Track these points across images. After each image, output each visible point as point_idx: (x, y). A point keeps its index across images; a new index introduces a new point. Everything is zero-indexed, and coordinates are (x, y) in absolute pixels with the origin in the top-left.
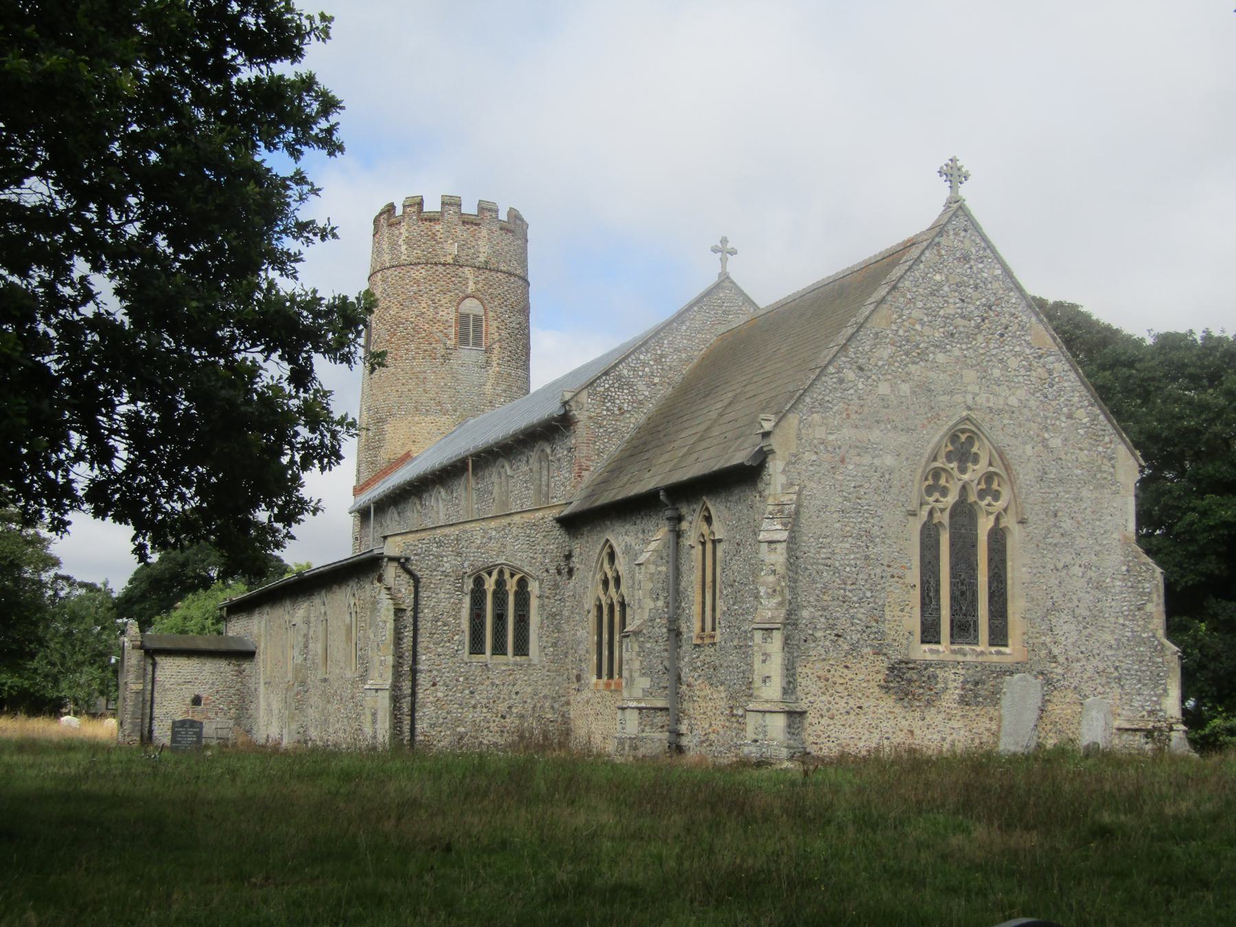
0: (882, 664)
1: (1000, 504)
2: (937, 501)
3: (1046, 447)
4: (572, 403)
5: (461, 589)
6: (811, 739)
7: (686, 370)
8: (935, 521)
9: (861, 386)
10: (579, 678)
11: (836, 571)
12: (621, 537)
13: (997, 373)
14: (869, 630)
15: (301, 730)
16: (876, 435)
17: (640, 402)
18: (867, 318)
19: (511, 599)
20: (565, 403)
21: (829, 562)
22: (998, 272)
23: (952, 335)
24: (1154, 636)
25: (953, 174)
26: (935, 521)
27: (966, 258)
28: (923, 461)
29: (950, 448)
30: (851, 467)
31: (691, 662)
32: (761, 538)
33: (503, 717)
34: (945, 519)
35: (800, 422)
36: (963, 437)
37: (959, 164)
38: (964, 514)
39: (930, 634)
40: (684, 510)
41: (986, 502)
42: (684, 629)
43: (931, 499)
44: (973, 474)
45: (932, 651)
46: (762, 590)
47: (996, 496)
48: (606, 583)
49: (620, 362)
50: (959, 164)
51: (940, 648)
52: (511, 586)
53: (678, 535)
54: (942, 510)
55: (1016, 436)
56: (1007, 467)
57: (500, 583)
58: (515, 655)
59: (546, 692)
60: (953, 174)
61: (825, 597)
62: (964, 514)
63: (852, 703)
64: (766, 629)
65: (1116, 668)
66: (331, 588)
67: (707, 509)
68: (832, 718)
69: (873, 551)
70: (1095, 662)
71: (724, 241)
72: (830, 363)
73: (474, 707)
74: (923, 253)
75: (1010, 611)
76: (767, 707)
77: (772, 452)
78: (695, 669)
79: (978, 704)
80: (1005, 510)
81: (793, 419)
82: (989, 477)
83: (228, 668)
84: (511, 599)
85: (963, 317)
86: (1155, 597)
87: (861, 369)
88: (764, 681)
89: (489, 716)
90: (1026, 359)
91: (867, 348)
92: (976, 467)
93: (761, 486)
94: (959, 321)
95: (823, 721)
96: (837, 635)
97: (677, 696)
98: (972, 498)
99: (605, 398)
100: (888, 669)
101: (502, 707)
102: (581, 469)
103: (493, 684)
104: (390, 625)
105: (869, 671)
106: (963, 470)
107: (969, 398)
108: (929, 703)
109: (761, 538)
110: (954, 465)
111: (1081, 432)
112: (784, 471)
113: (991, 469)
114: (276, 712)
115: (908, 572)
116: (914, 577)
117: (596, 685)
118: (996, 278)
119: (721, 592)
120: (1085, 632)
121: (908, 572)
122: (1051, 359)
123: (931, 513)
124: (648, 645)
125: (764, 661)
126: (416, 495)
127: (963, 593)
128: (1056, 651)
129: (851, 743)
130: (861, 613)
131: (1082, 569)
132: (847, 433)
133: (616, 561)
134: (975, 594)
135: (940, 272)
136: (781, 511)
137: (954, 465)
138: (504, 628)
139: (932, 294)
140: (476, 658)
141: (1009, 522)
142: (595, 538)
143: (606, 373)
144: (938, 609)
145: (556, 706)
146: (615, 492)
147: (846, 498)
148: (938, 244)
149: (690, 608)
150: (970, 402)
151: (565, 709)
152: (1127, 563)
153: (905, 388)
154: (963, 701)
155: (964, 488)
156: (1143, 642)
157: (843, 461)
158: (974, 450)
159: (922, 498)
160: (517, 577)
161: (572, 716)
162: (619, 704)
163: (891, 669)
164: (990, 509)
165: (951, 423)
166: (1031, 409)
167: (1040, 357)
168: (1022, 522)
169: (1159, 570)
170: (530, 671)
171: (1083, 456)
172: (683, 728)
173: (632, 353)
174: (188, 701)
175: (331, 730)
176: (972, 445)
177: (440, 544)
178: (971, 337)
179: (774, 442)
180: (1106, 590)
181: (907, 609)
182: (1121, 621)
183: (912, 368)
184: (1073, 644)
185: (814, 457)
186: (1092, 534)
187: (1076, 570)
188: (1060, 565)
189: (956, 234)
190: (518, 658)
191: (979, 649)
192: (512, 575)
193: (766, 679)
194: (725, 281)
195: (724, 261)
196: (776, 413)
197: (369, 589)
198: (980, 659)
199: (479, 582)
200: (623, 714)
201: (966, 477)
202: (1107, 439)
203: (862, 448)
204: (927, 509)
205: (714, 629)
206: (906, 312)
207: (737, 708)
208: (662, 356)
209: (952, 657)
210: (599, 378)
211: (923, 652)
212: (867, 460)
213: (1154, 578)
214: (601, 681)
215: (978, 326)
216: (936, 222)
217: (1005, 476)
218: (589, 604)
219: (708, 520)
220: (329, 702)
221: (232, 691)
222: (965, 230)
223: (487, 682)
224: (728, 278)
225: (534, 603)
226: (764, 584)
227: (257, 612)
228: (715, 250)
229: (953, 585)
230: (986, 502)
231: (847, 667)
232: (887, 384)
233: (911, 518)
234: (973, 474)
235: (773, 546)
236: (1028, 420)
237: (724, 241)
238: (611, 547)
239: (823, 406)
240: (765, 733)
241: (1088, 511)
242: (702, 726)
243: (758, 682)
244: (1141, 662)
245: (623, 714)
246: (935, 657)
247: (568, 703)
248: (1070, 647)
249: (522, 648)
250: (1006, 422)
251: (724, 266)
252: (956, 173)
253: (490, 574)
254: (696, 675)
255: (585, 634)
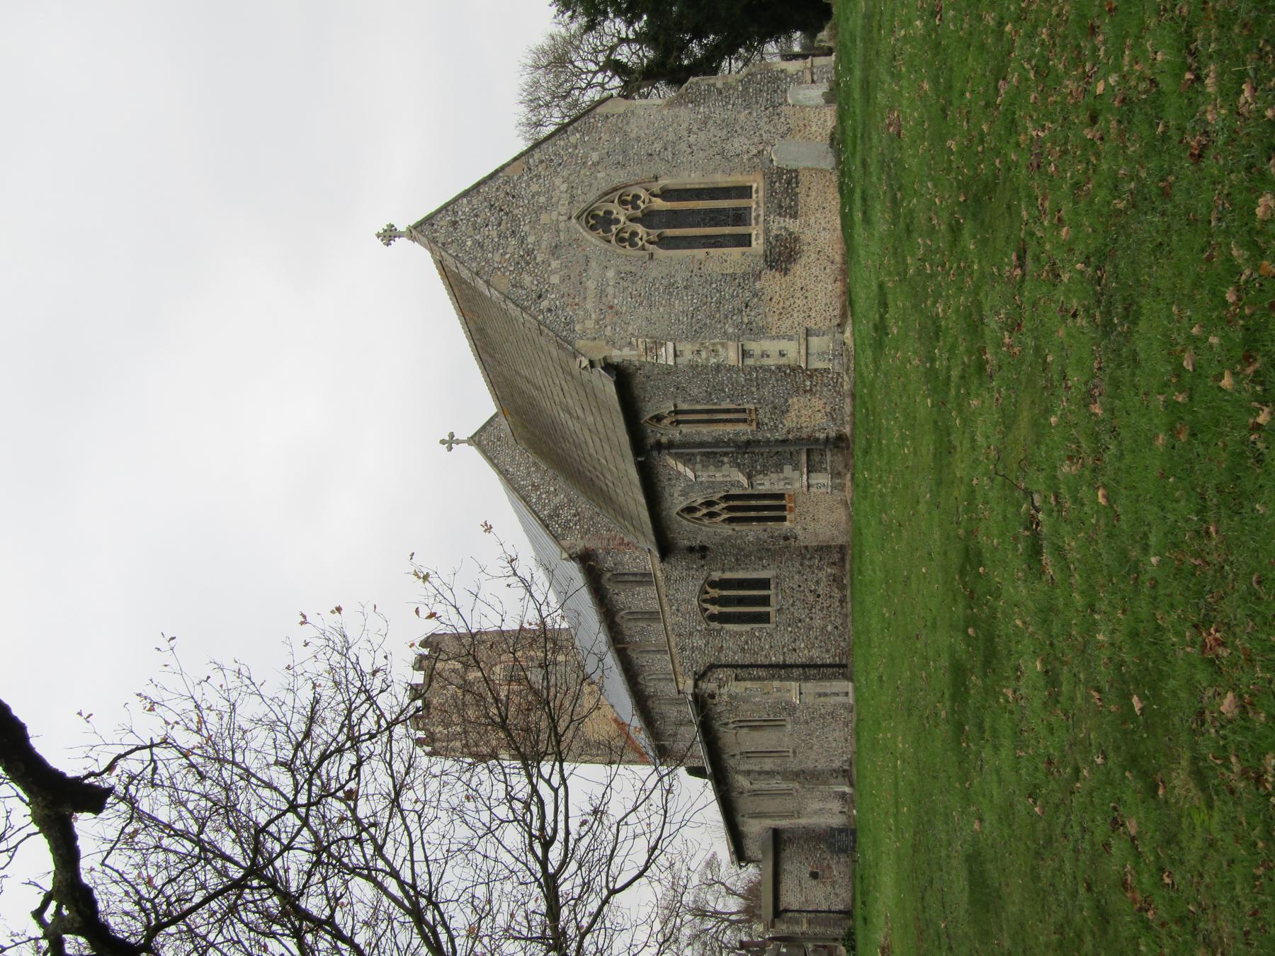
0: (768, 274)
1: (643, 194)
2: (641, 239)
3: (598, 163)
4: (571, 552)
5: (719, 632)
6: (827, 323)
7: (543, 466)
8: (656, 239)
9: (553, 296)
10: (786, 538)
11: (697, 309)
12: (675, 501)
13: (542, 199)
14: (742, 285)
15: (835, 775)
16: (591, 284)
17: (570, 501)
18: (500, 293)
19: (725, 593)
20: (571, 557)
21: (690, 316)
22: (465, 201)
23: (513, 232)
24: (741, 81)
25: (389, 235)
26: (656, 239)
27: (455, 223)
28: (610, 249)
29: (600, 230)
30: (616, 301)
31: (770, 430)
32: (672, 364)
33: (819, 596)
34: (655, 233)
35: (581, 338)
36: (592, 222)
37: (381, 231)
38: (649, 218)
39: (744, 241)
40: (651, 441)
41: (641, 205)
42: (744, 438)
43: (640, 243)
44: (620, 213)
45: (756, 240)
46: (713, 361)
47: (637, 197)
48: (711, 515)
49: (538, 517)
50: (381, 231)
51: (754, 233)
52: (715, 593)
53: (671, 445)
54: (648, 234)
55: (590, 185)
56: (615, 190)
57: (713, 601)
58: (769, 589)
59: (797, 565)
60: (389, 235)
61: (717, 316)
62: (649, 218)
63: (798, 294)
64: (743, 355)
65: (766, 109)
66: (720, 748)
67: (651, 419)
68: (811, 309)
69: (681, 284)
70: (762, 123)
71: (443, 442)
72: (535, 319)
73: (811, 619)
74: (450, 255)
75: (725, 185)
76: (803, 352)
77: (605, 359)
78: (776, 427)
79: (796, 205)
80: (647, 190)
81: (580, 344)
82: (623, 202)
83: (788, 851)
84: (725, 593)
85: (499, 225)
86: (711, 81)
87: (540, 297)
88: (784, 355)
89: (818, 607)
90: (531, 179)
91: (524, 292)
92: (615, 212)
93: (632, 369)
94: (503, 227)
95: (813, 315)
96: (746, 307)
97: (799, 441)
98: (639, 213)
99: (566, 527)
100: (771, 270)
101: (811, 598)
102: (622, 543)
103: (793, 605)
104: (749, 684)
105: (772, 283)
106: (617, 221)
107: (561, 218)
108: (797, 240)
109: (672, 364)
110: (613, 228)
111: (586, 139)
112: (620, 349)
113: (616, 201)
114: (821, 805)
115: (697, 257)
116: (700, 253)
117: (791, 521)
118: (469, 202)
119: (715, 404)
120: (739, 131)
121: (697, 257)
122: (531, 161)
123: (651, 243)
124: (759, 467)
125: (768, 356)
126: (646, 701)
127: (712, 219)
128: (755, 152)
129: (829, 294)
130: (728, 291)
131: (691, 135)
132: (589, 305)
133: (694, 505)
134: (712, 211)
135: (464, 243)
136: (651, 349)
137: (613, 228)
138: (749, 597)
139: (482, 247)
140: (773, 619)
141: (656, 188)
142: (676, 526)
143: (547, 526)
144: (724, 236)
145: (808, 556)
146: (640, 509)
147: (641, 304)
148: (443, 244)
149: (729, 433)
150: (565, 218)
151: (810, 549)
152: (686, 104)
153: (555, 264)
154: (795, 216)
155: (632, 220)
156: (746, 89)
157: (611, 307)
158: (601, 214)
159: (639, 249)
160: (709, 589)
161: (816, 544)
162: (805, 489)
163: (771, 267)
164: (647, 201)
165: (581, 231)
166: (570, 175)
167: (530, 169)
168: (656, 178)
169: (692, 79)
170: (782, 577)
171: (605, 137)
172: (822, 436)
173: (531, 507)
174: (815, 882)
175: (834, 745)
176: (598, 215)
177: (683, 649)
178: (514, 219)
179: (598, 357)
180: (707, 118)
181: (724, 257)
182: (730, 106)
183: (539, 259)
184: (749, 139)
185: (609, 328)
186: (665, 129)
187: (692, 139)
188: (689, 150)
189: (436, 231)
190: (772, 586)
191: (754, 206)
192: (707, 592)
193: (782, 354)
194: (476, 440)
195: (458, 442)
196: (575, 357)
197: (720, 707)
198: (762, 204)
199: (712, 618)
200: (813, 486)
201: (622, 219)
202: (592, 120)
203: (602, 293)
204: (647, 245)
205: (744, 411)
206: (496, 265)
207: (805, 386)
208: (533, 485)
209: (761, 225)
210: (551, 532)
211: (758, 245)
212: (610, 290)
213: (697, 83)
214: (788, 517)
215: (507, 214)
216: (426, 247)
217: (622, 191)
218: (727, 530)
219: (659, 418)
220: (811, 748)
221: (806, 847)
222: (433, 225)
223: (792, 609)
224: (472, 437)
225: (728, 575)
226: (708, 359)
227: (741, 828)
228: (450, 449)
229: (705, 226)
230: (641, 205)
231: (771, 299)
232: (552, 277)
233: (655, 257)
234: (620, 213)
235: (678, 353)
236: (578, 176)
237: (443, 442)
238: (683, 510)
239: (569, 323)
240: (823, 353)
241: (647, 132)
242: (820, 419)
243: (783, 361)
244: (761, 91)
245: (813, 486)
246: (761, 237)
247: (806, 547)
248: (751, 142)
249: (764, 584)
250: (580, 192)
251: (463, 442)
252: (387, 234)
253: (706, 610)
254: (781, 426)
255: (752, 533)
